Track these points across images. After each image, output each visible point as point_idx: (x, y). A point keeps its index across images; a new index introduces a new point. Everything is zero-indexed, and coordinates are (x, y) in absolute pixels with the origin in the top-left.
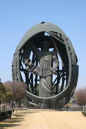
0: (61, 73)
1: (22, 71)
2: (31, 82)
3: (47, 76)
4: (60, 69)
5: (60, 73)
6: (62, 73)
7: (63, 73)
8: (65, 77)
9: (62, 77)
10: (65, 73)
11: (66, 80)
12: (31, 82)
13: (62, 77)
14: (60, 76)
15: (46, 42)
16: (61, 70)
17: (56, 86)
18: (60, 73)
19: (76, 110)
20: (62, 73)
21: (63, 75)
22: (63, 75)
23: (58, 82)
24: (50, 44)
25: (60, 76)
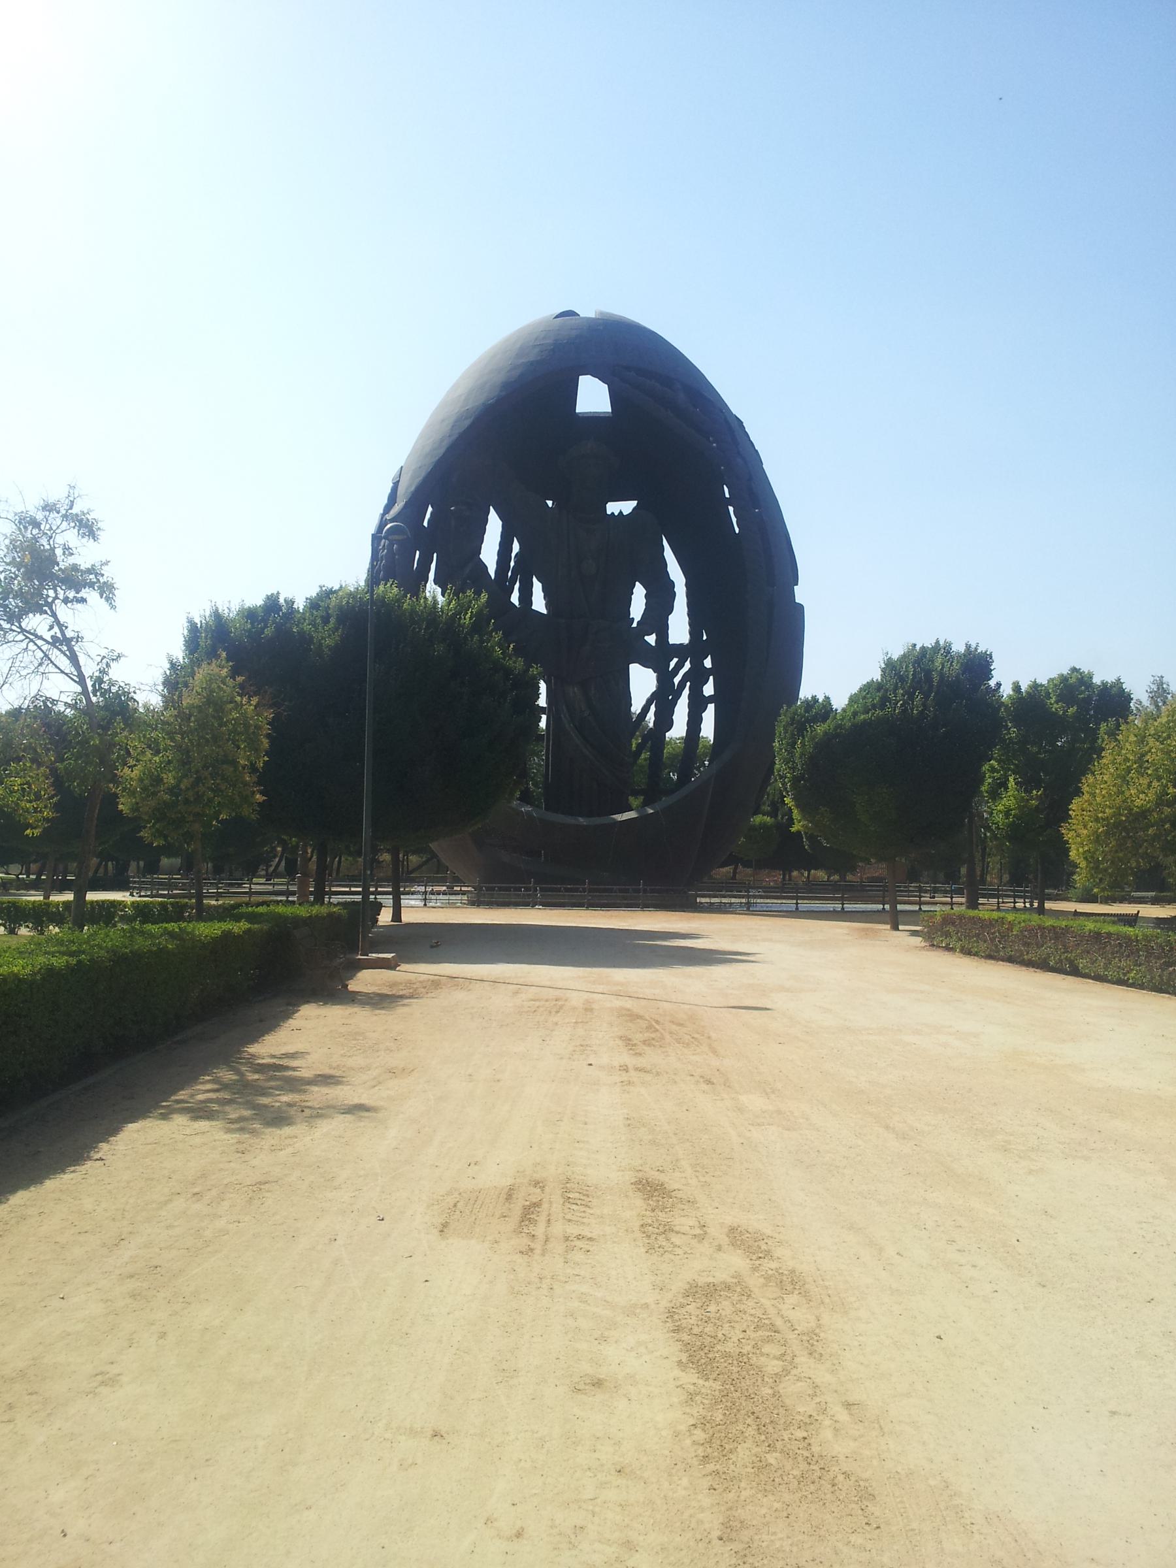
6: (687, 665)
9: (686, 692)
10: (708, 663)
13: (686, 692)
14: (677, 680)
20: (687, 665)
22: (697, 677)
25: (677, 680)
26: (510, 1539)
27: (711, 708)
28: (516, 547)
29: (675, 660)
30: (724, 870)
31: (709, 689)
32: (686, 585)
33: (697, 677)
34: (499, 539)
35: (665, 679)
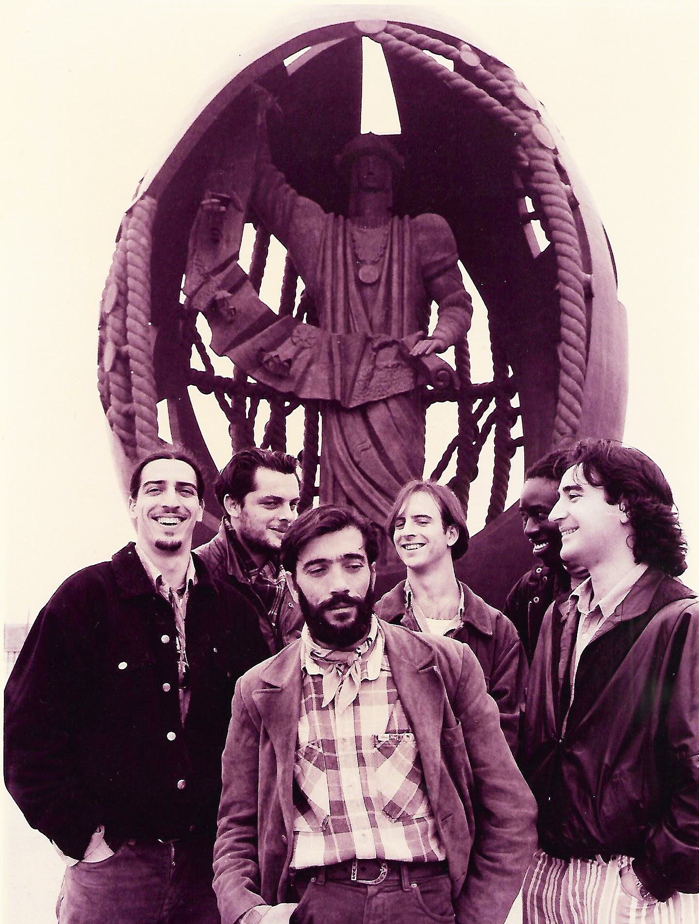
0: (483, 407)
1: (205, 390)
3: (376, 403)
4: (365, 128)
5: (475, 407)
6: (492, 406)
7: (503, 404)
8: (517, 431)
9: (492, 436)
10: (515, 402)
13: (492, 436)
14: (481, 423)
15: (437, 220)
17: (455, 455)
18: (475, 407)
20: (492, 406)
21: (504, 418)
22: (504, 418)
23: (468, 471)
24: (535, 185)
25: (481, 423)
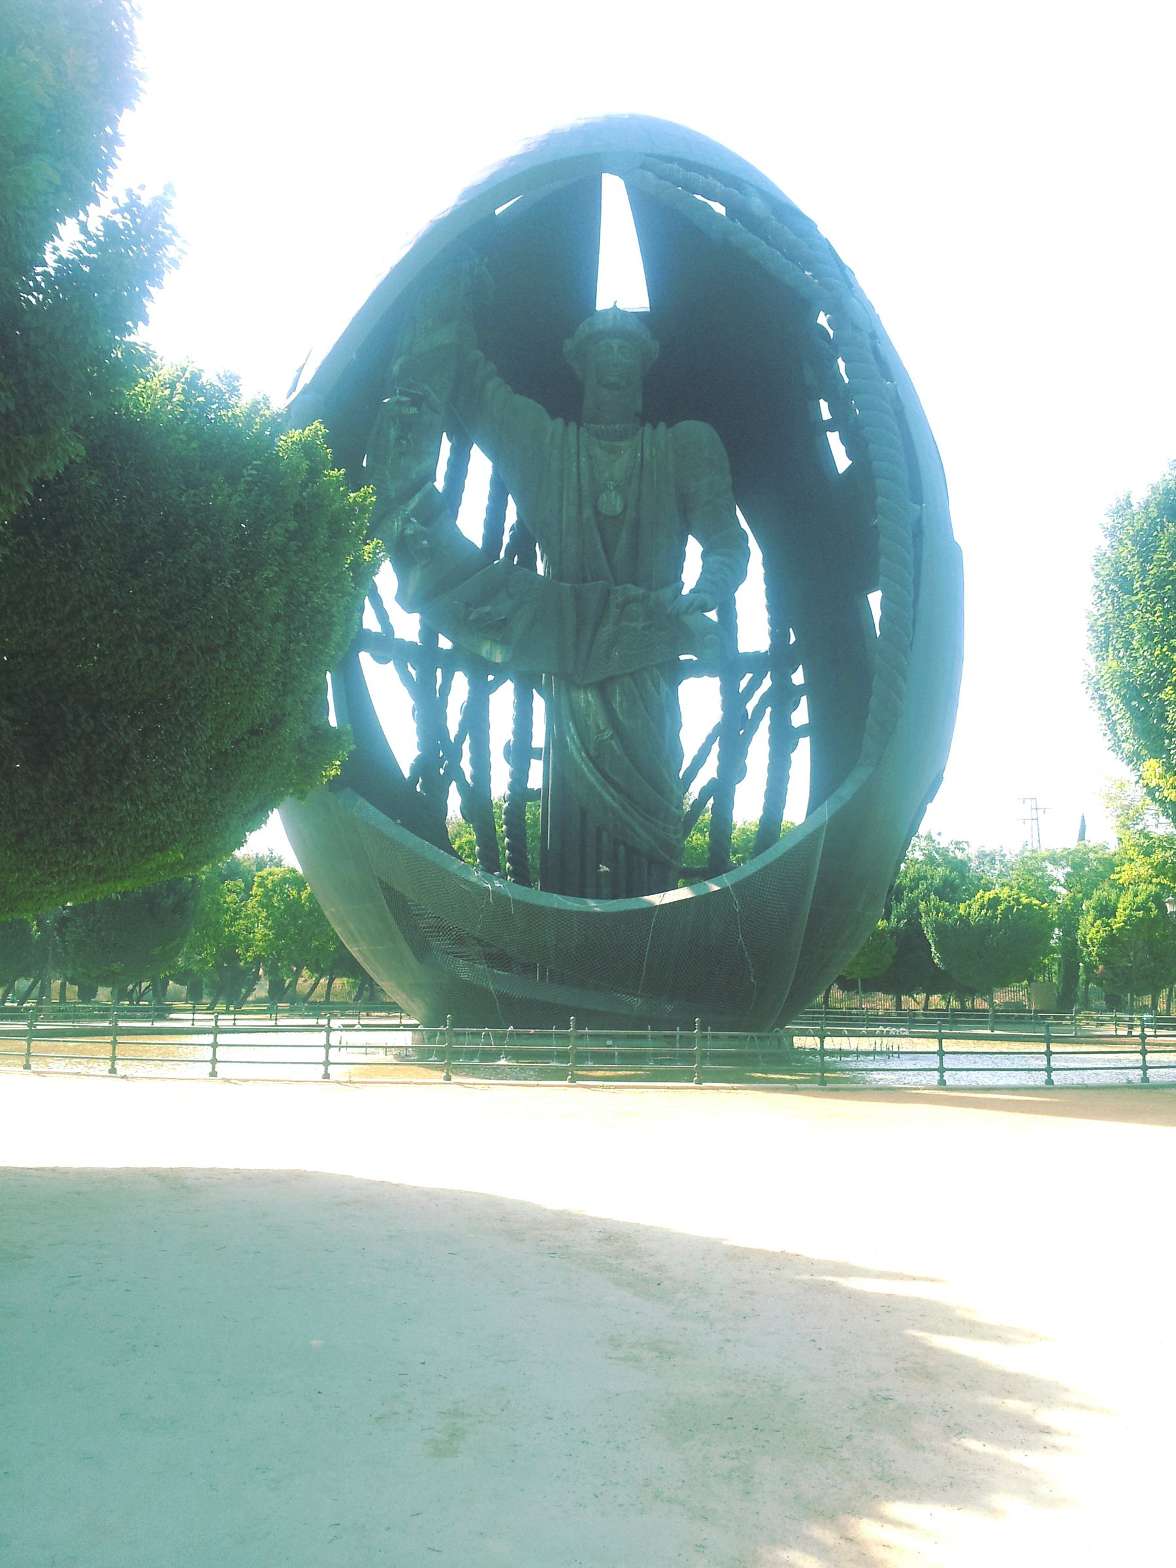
1: (382, 660)
2: (466, 766)
5: (744, 683)
6: (767, 683)
9: (766, 722)
10: (798, 678)
11: (804, 699)
12: (466, 766)
13: (766, 722)
14: (750, 706)
16: (757, 656)
17: (716, 748)
18: (744, 683)
19: (963, 1321)
20: (767, 683)
22: (783, 699)
23: (732, 768)
25: (750, 706)
26: (611, 679)
27: (805, 744)
28: (511, 515)
29: (749, 676)
30: (335, 472)
31: (800, 716)
32: (769, 608)
33: (783, 699)
34: (467, 482)
35: (733, 701)
